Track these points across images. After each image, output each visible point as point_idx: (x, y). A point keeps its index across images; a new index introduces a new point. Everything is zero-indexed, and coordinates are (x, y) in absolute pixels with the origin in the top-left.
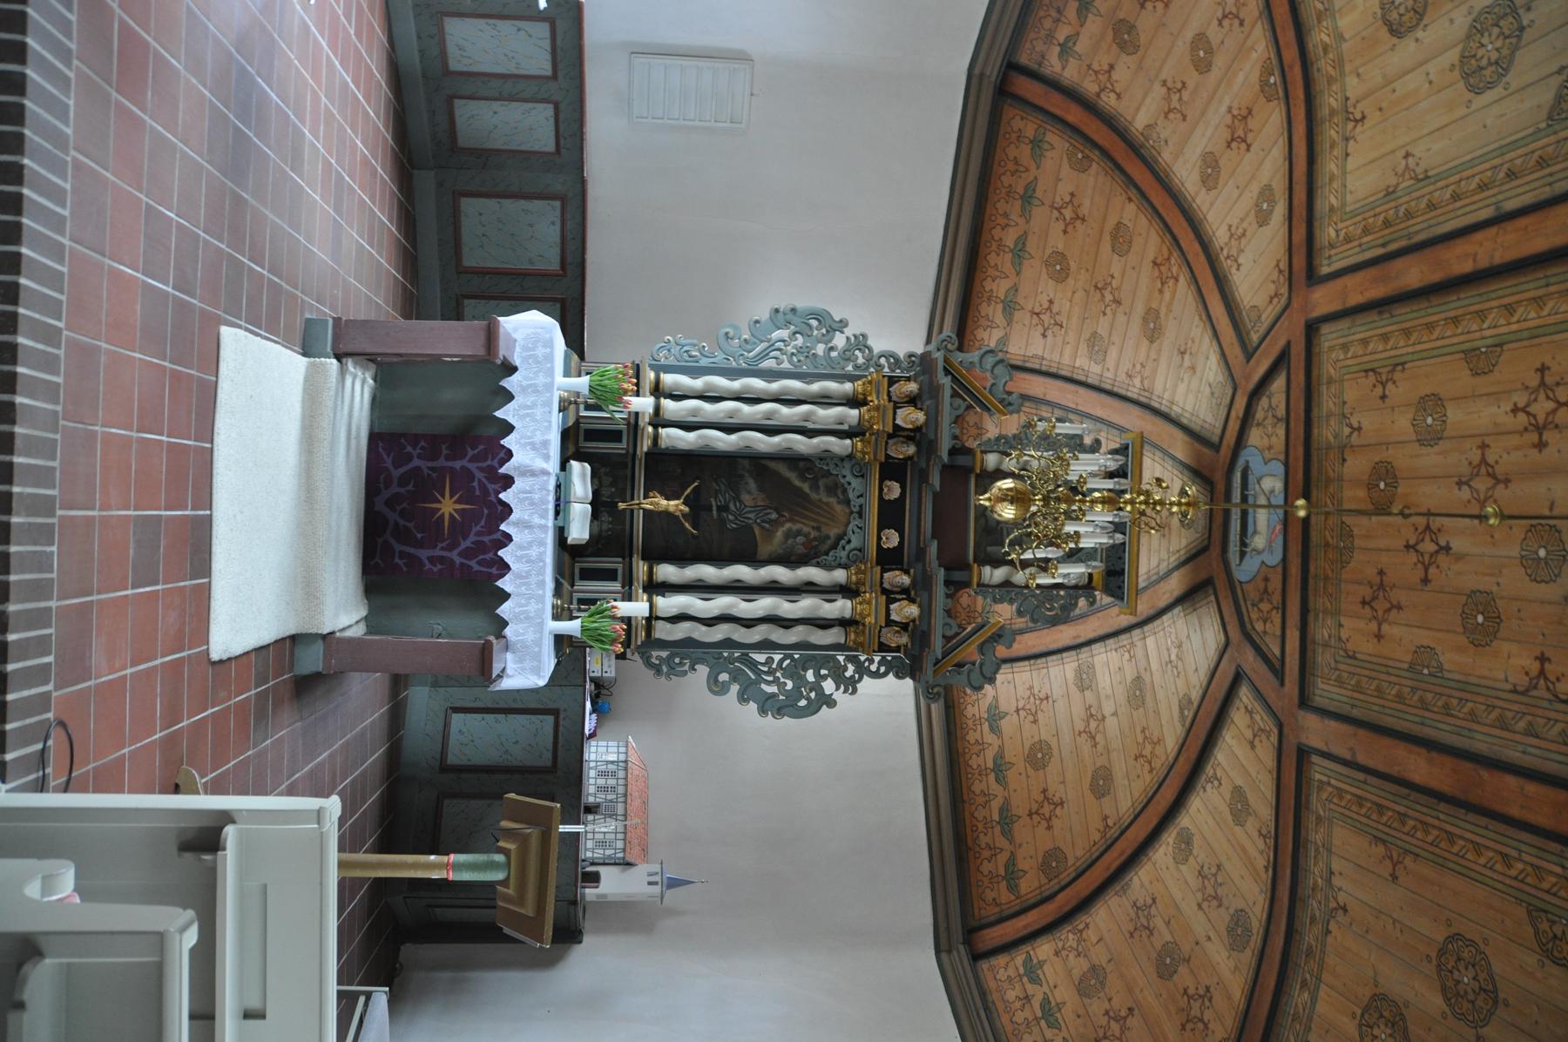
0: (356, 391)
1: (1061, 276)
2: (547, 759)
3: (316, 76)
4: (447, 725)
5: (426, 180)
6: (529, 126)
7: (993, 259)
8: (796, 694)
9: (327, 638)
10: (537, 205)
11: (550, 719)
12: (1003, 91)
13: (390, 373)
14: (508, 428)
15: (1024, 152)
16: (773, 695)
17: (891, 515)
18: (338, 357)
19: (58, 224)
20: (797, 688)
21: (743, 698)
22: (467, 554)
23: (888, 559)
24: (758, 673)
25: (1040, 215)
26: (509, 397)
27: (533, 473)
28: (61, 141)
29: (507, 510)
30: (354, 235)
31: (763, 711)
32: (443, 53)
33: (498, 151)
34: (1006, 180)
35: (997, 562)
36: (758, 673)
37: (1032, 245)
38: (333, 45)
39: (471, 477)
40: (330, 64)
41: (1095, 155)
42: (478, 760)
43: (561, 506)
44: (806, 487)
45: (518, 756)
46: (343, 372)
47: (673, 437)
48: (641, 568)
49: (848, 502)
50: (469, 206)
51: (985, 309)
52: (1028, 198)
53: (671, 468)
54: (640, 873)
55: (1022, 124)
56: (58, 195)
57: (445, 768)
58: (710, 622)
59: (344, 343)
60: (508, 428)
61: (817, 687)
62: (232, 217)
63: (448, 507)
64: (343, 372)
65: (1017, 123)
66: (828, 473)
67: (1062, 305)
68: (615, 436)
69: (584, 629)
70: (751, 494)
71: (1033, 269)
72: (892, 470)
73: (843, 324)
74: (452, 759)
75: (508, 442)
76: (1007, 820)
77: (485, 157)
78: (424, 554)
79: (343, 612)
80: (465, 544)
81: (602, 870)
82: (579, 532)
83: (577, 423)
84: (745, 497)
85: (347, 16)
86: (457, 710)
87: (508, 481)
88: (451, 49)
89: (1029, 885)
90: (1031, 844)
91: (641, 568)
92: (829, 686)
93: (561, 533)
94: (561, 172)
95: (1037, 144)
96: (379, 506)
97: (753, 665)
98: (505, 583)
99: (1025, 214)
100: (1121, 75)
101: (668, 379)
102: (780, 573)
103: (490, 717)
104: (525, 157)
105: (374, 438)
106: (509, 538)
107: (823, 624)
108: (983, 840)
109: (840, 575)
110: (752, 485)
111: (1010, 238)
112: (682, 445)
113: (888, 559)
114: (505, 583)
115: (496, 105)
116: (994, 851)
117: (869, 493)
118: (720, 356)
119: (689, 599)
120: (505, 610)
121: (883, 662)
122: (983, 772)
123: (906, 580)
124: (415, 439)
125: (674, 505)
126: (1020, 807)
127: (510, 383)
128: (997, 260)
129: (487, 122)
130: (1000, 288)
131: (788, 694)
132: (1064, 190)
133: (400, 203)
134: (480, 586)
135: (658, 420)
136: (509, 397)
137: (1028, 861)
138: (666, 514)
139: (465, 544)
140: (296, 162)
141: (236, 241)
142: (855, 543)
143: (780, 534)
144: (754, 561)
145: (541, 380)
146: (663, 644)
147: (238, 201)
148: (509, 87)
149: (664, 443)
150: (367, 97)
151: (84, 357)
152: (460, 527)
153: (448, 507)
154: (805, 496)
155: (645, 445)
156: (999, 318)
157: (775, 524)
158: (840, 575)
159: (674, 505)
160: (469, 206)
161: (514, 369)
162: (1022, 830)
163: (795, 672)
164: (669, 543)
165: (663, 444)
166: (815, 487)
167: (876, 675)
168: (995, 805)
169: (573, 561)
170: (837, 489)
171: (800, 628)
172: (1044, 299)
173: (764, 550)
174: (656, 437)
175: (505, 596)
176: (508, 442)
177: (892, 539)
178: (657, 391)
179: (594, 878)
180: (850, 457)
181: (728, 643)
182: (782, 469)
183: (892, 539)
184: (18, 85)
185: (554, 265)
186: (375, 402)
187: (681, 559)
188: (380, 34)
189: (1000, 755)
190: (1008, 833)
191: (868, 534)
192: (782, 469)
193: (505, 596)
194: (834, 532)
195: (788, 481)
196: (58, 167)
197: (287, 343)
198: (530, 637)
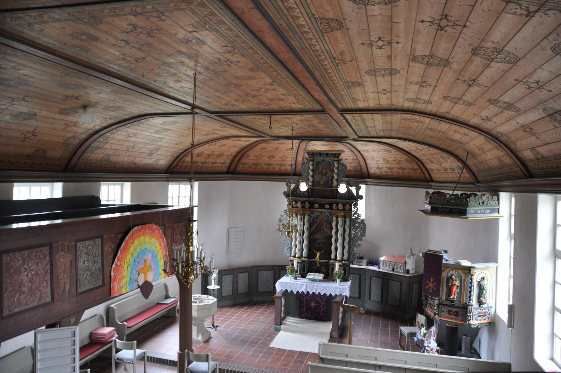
0: (290, 321)
1: (274, 157)
2: (380, 279)
3: (232, 325)
4: (373, 301)
5: (255, 299)
6: (243, 278)
7: (271, 170)
8: (361, 228)
9: (331, 331)
10: (259, 276)
11: (372, 278)
12: (233, 173)
13: (288, 313)
14: (298, 292)
15: (246, 166)
16: (361, 233)
17: (322, 206)
18: (281, 324)
19: (248, 369)
20: (359, 228)
21: (361, 240)
22: (322, 301)
23: (331, 208)
24: (356, 236)
25: (259, 162)
26: (292, 291)
27: (306, 287)
28: (238, 367)
29: (313, 293)
30: (262, 318)
31: (364, 236)
32: (229, 296)
33: (249, 284)
34: (252, 169)
35: (333, 183)
36: (356, 236)
37: (268, 163)
38: (227, 321)
39: (307, 300)
40: (230, 322)
41: (246, 154)
42: (380, 295)
43: (314, 280)
44: (316, 224)
45: (380, 286)
46: (284, 324)
47: (305, 253)
48: (332, 261)
49: (319, 216)
50: (260, 289)
51: (283, 170)
52: (256, 164)
53: (311, 255)
54: (408, 260)
55: (240, 168)
56: (245, 368)
57: (382, 302)
58: (344, 247)
59: (279, 322)
60: (298, 292)
61: (359, 223)
62: (253, 343)
63: (313, 304)
64: (284, 324)
65: (240, 169)
66: (313, 220)
67: (280, 156)
68: (304, 266)
69: (338, 278)
70: (318, 236)
71: (272, 162)
72: (312, 206)
73: (282, 216)
74: (380, 301)
75: (300, 292)
76: (401, 168)
77: (250, 287)
78: (322, 310)
79: (327, 327)
80: (320, 301)
81: (407, 269)
82: (320, 276)
83: (300, 274)
84: (318, 237)
85: (222, 317)
86: (370, 298)
87: (308, 292)
88: (228, 294)
89: (416, 167)
90: (405, 164)
91: (332, 261)
92: (359, 221)
93: (320, 281)
94: (253, 271)
95: (244, 164)
96: (313, 317)
97: (354, 237)
98: (328, 294)
99: (260, 164)
100: (228, 154)
101: (293, 254)
102: (333, 231)
103: (372, 291)
104: (249, 278)
105: (300, 317)
106: (319, 293)
107: (345, 223)
108: (407, 174)
109: (334, 218)
110: (316, 236)
111: (266, 167)
112: (306, 251)
113: (331, 208)
114: (328, 294)
115: (239, 285)
116: (408, 173)
117: (317, 211)
118: (288, 242)
119: (338, 252)
120: (333, 295)
121: (354, 208)
122: (392, 172)
123: (335, 205)
124: (300, 310)
125: (318, 254)
126: (399, 166)
127: (289, 291)
128: (271, 169)
129: (242, 286)
130: (277, 167)
131: (361, 230)
132: (254, 158)
133: (259, 305)
134: (328, 300)
135: (301, 256)
136: (292, 291)
137: (410, 166)
138: (320, 256)
139: (320, 301)
140: (246, 330)
141: (257, 343)
142: (328, 214)
143: (326, 230)
144: (331, 237)
145: (289, 285)
146: (349, 257)
147: (251, 342)
148: (235, 282)
149: (306, 256)
150: (237, 313)
151: (266, 367)
152: (317, 302)
153: (313, 304)
154: (318, 224)
155: (306, 259)
156: (285, 167)
157: (324, 231)
158: (334, 218)
159: (318, 254)
160: (260, 289)
161: (287, 290)
162: (403, 166)
163: (356, 228)
164: (327, 254)
165: (306, 256)
166: (316, 222)
167: (357, 210)
168: (399, 171)
169: (329, 277)
170: (316, 218)
171: (346, 228)
172: (279, 159)
173: (329, 234)
174: (305, 257)
175: (330, 294)
176: (300, 292)
177: (327, 206)
178: (295, 257)
179: (408, 271)
180: (309, 215)
181: (349, 243)
182: (312, 229)
183: (327, 206)
184: (231, 371)
185: (272, 272)
186: (293, 316)
187: (331, 252)
188: (225, 309)
189: (387, 168)
190: (405, 169)
191: (326, 212)
192: (312, 229)
193: (330, 294)
194: (326, 219)
195: (315, 228)
196: (241, 368)
197: (277, 334)
198: (339, 290)
